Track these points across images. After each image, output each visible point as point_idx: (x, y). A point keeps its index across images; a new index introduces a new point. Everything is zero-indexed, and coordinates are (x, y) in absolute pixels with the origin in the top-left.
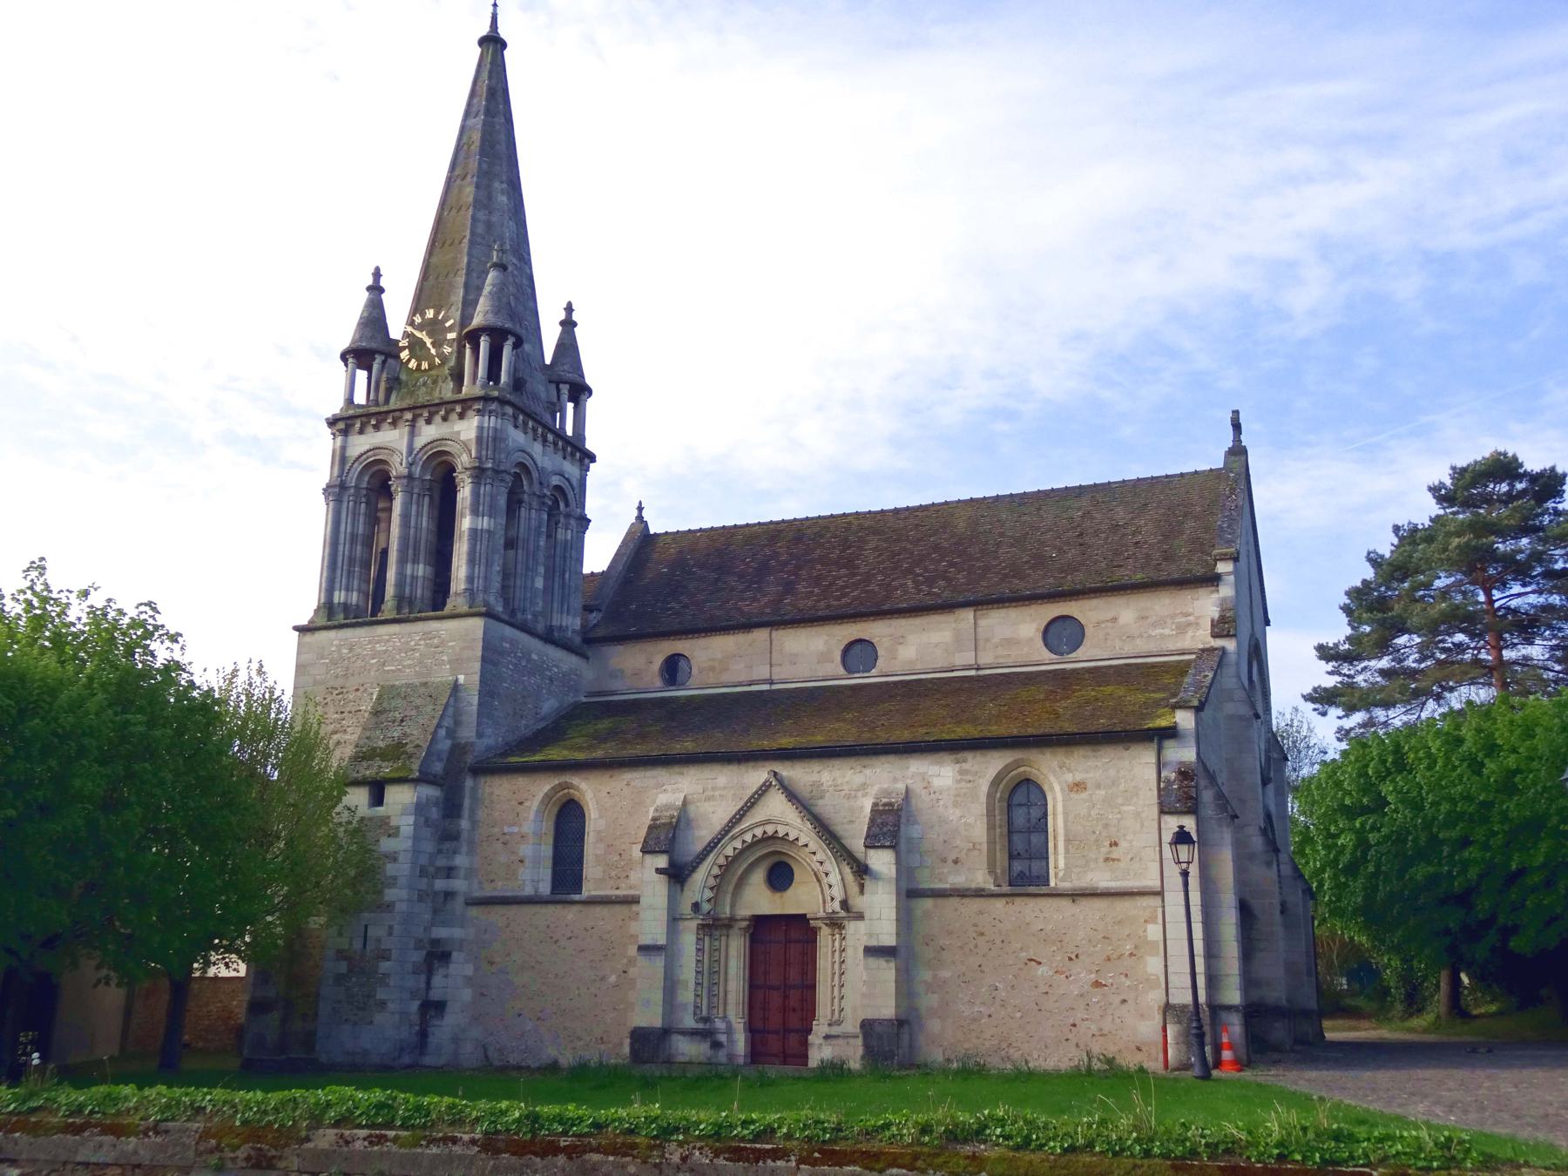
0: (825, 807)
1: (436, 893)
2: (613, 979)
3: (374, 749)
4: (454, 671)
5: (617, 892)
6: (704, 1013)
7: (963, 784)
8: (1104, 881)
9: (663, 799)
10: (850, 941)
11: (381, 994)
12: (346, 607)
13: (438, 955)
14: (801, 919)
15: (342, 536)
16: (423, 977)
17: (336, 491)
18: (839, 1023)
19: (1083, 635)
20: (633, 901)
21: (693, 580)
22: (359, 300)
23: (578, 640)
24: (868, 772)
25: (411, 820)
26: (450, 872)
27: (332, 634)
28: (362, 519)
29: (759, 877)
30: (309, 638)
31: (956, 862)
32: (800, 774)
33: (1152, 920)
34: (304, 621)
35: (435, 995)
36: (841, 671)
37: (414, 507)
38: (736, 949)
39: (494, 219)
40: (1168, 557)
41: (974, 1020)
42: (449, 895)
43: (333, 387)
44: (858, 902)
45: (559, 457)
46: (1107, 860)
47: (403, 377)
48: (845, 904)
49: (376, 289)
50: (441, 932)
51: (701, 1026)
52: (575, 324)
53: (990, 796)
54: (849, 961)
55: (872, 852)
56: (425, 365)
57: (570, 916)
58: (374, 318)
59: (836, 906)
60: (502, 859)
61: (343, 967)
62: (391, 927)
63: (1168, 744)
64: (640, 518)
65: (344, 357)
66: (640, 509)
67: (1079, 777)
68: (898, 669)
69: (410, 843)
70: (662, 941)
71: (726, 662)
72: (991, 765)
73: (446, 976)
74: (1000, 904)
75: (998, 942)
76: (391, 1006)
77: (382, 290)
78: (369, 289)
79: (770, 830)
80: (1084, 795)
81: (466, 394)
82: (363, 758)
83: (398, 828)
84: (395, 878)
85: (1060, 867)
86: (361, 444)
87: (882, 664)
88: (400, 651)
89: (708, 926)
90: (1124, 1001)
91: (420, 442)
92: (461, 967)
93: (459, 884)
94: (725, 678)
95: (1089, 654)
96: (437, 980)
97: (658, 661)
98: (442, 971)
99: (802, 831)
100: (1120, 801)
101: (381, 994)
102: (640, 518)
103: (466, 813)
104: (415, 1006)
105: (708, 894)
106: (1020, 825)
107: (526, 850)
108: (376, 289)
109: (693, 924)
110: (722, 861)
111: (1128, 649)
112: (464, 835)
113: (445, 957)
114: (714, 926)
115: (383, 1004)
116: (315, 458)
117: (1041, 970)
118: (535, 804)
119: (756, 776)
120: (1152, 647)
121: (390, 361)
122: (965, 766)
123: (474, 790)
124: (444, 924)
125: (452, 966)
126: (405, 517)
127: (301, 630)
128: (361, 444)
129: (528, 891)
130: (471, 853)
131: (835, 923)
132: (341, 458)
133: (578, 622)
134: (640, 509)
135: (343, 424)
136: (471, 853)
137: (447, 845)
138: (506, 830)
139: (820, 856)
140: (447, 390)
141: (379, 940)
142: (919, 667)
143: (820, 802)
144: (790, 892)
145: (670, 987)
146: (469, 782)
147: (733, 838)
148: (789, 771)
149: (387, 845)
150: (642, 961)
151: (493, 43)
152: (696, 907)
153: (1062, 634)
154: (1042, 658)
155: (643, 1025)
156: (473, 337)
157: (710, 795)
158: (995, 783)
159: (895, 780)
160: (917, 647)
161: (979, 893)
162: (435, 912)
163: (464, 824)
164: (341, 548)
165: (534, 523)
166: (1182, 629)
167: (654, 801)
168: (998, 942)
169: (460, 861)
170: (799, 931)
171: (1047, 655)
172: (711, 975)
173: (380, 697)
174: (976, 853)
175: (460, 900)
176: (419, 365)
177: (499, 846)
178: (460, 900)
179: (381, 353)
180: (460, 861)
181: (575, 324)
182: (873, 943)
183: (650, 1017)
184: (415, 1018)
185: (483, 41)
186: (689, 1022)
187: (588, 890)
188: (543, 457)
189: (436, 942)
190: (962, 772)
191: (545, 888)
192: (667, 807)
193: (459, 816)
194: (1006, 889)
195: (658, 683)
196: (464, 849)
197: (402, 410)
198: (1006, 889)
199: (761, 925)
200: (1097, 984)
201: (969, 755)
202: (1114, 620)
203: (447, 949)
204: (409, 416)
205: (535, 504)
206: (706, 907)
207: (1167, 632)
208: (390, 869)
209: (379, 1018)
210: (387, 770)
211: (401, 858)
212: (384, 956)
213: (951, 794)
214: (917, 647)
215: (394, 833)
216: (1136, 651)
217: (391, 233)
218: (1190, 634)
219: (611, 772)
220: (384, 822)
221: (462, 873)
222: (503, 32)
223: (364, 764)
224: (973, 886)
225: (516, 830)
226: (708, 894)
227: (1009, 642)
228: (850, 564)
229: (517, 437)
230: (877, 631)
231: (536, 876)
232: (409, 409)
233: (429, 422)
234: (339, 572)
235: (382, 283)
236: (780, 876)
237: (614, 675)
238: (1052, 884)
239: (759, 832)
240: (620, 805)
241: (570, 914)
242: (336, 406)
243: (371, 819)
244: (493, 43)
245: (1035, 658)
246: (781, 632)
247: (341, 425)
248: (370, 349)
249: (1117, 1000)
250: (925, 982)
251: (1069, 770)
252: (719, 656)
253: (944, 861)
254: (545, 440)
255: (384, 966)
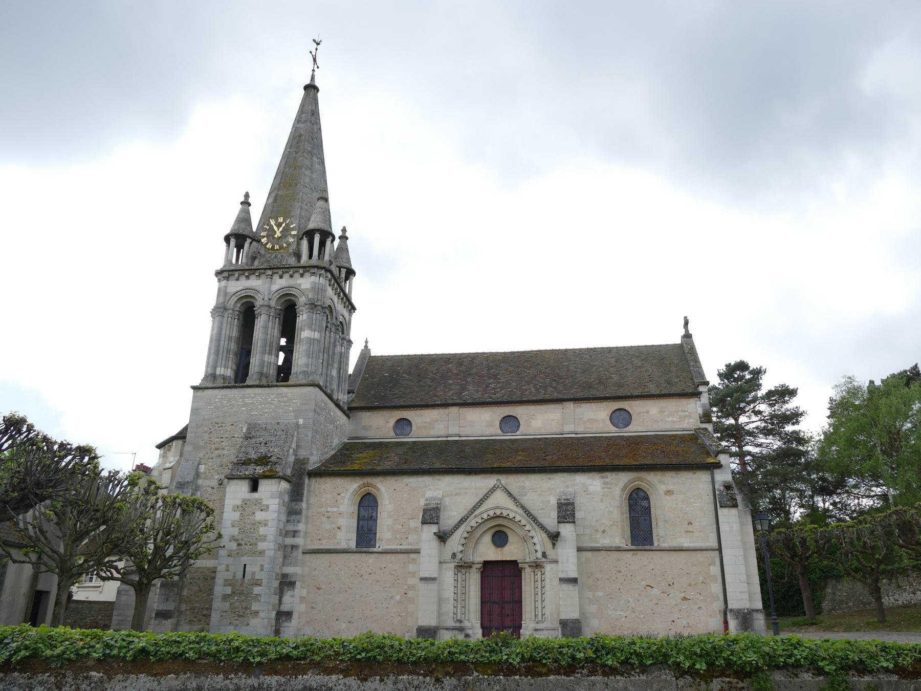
0: (526, 500)
1: (285, 546)
2: (398, 597)
3: (250, 459)
4: (297, 417)
5: (401, 547)
6: (459, 617)
7: (606, 490)
8: (686, 544)
9: (429, 494)
10: (548, 575)
11: (255, 607)
12: (224, 378)
13: (286, 583)
14: (515, 562)
15: (223, 337)
16: (278, 597)
17: (219, 311)
18: (542, 622)
19: (611, 420)
20: (417, 552)
21: (400, 382)
22: (236, 209)
23: (346, 408)
24: (552, 482)
25: (277, 501)
26: (295, 533)
27: (217, 391)
28: (235, 328)
29: (488, 538)
30: (200, 393)
31: (604, 532)
32: (514, 482)
33: (713, 564)
34: (197, 383)
35: (285, 608)
36: (499, 432)
37: (270, 323)
38: (474, 580)
39: (314, 176)
40: (668, 382)
41: (617, 619)
42: (293, 547)
43: (218, 254)
44: (551, 553)
45: (342, 306)
46: (687, 531)
47: (262, 252)
48: (544, 555)
49: (246, 203)
50: (289, 570)
51: (458, 625)
52: (347, 238)
53: (621, 496)
54: (547, 587)
55: (562, 525)
56: (269, 246)
57: (371, 560)
58: (244, 218)
59: (539, 555)
60: (328, 526)
61: (228, 590)
62: (262, 566)
63: (716, 471)
64: (366, 346)
65: (227, 239)
66: (366, 342)
67: (670, 487)
68: (532, 432)
69: (276, 515)
70: (434, 575)
71: (432, 425)
72: (620, 482)
73: (292, 596)
74: (629, 555)
75: (629, 576)
76: (262, 614)
77: (249, 205)
78: (242, 203)
79: (498, 512)
80: (672, 497)
81: (284, 270)
82: (243, 464)
83: (268, 506)
84: (265, 536)
85: (662, 534)
86: (237, 286)
87: (522, 429)
88: (261, 403)
89: (461, 566)
90: (700, 608)
91: (275, 288)
92: (299, 591)
93: (299, 541)
94: (432, 433)
95: (636, 428)
96: (287, 598)
97: (392, 422)
98: (290, 593)
99: (519, 516)
100: (692, 500)
101: (255, 607)
102: (366, 346)
103: (305, 498)
104: (274, 614)
105: (461, 548)
106: (639, 512)
107: (342, 522)
108: (246, 203)
109: (452, 565)
110: (469, 529)
111: (655, 427)
112: (304, 512)
113: (292, 584)
114: (463, 567)
115: (257, 613)
116: (208, 292)
117: (655, 591)
118: (348, 495)
119: (489, 481)
120: (668, 427)
121: (254, 243)
122: (606, 480)
123: (309, 486)
124: (291, 564)
125: (296, 590)
126: (266, 328)
127: (194, 388)
128: (237, 286)
129: (343, 546)
130: (307, 523)
131: (537, 565)
132: (222, 292)
133: (346, 397)
134: (366, 342)
135: (224, 274)
136: (307, 523)
137: (293, 517)
138: (329, 509)
139: (527, 528)
140: (292, 261)
141: (254, 574)
142: (543, 431)
143: (525, 498)
144: (507, 548)
145: (440, 601)
146: (307, 481)
147: (476, 516)
148: (506, 480)
149: (260, 516)
150: (423, 586)
151: (311, 89)
152: (454, 555)
153: (621, 418)
154: (610, 430)
155: (423, 624)
156: (310, 234)
157: (458, 494)
158: (624, 489)
159: (567, 487)
160: (542, 422)
161: (618, 549)
162: (285, 557)
163: (304, 505)
164: (222, 343)
165: (332, 340)
166: (682, 418)
167: (423, 496)
168: (629, 576)
169: (301, 527)
170: (512, 569)
171: (613, 429)
172: (461, 595)
173: (248, 429)
174: (614, 527)
175: (300, 550)
176: (273, 247)
177: (325, 519)
178: (300, 550)
179: (250, 238)
180: (301, 527)
181: (347, 238)
182: (564, 576)
183: (429, 620)
184: (273, 622)
185: (306, 88)
186: (451, 623)
187: (381, 545)
188: (340, 307)
189: (284, 576)
190: (605, 483)
191: (353, 545)
192: (434, 499)
193: (302, 501)
194: (630, 547)
195: (392, 434)
196: (303, 520)
197: (265, 269)
198: (630, 547)
199: (488, 566)
200: (685, 599)
201: (608, 474)
202: (647, 412)
203: (293, 580)
204: (269, 272)
205: (333, 330)
206: (459, 556)
207: (675, 419)
208: (262, 530)
209: (253, 622)
210: (260, 470)
211: (270, 524)
212: (258, 583)
213: (600, 497)
214: (542, 422)
215: (265, 509)
216: (660, 429)
217: (254, 177)
218: (686, 421)
219: (396, 478)
220: (258, 502)
221: (302, 534)
222: (317, 83)
223: (244, 467)
224: (614, 545)
225: (336, 509)
226: (461, 548)
227: (591, 421)
228: (495, 377)
229: (330, 292)
230: (519, 411)
231: (347, 537)
232: (270, 269)
233: (281, 277)
234: (220, 357)
235: (250, 200)
236: (500, 539)
237: (365, 428)
238: (656, 544)
239: (491, 513)
240: (401, 499)
241: (370, 559)
242: (220, 265)
243: (249, 500)
244: (311, 89)
245: (607, 429)
246: (464, 409)
247: (226, 274)
248: (238, 238)
249: (696, 607)
250: (589, 599)
251: (664, 484)
252: (429, 420)
253: (597, 531)
254: (339, 296)
255: (257, 590)
